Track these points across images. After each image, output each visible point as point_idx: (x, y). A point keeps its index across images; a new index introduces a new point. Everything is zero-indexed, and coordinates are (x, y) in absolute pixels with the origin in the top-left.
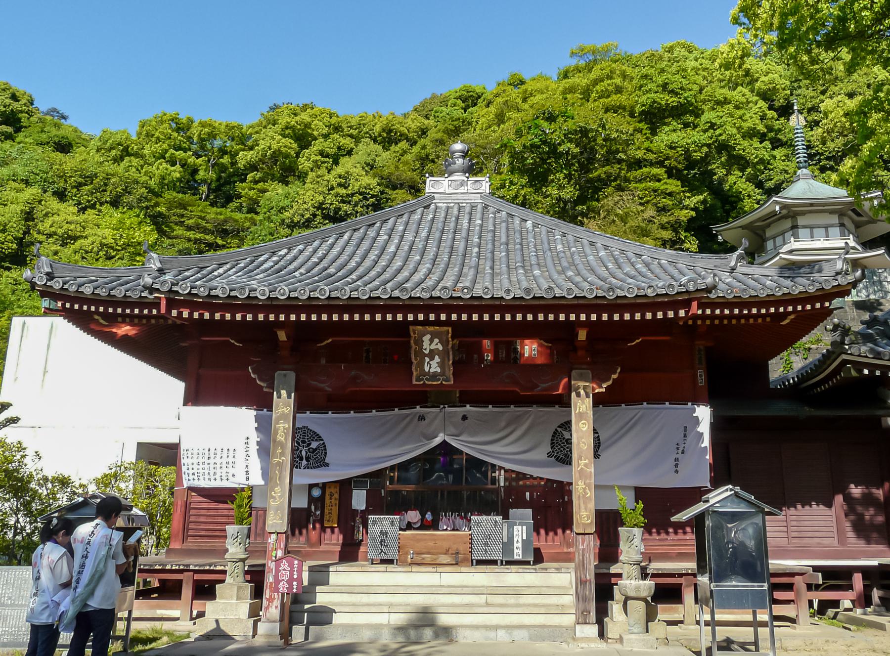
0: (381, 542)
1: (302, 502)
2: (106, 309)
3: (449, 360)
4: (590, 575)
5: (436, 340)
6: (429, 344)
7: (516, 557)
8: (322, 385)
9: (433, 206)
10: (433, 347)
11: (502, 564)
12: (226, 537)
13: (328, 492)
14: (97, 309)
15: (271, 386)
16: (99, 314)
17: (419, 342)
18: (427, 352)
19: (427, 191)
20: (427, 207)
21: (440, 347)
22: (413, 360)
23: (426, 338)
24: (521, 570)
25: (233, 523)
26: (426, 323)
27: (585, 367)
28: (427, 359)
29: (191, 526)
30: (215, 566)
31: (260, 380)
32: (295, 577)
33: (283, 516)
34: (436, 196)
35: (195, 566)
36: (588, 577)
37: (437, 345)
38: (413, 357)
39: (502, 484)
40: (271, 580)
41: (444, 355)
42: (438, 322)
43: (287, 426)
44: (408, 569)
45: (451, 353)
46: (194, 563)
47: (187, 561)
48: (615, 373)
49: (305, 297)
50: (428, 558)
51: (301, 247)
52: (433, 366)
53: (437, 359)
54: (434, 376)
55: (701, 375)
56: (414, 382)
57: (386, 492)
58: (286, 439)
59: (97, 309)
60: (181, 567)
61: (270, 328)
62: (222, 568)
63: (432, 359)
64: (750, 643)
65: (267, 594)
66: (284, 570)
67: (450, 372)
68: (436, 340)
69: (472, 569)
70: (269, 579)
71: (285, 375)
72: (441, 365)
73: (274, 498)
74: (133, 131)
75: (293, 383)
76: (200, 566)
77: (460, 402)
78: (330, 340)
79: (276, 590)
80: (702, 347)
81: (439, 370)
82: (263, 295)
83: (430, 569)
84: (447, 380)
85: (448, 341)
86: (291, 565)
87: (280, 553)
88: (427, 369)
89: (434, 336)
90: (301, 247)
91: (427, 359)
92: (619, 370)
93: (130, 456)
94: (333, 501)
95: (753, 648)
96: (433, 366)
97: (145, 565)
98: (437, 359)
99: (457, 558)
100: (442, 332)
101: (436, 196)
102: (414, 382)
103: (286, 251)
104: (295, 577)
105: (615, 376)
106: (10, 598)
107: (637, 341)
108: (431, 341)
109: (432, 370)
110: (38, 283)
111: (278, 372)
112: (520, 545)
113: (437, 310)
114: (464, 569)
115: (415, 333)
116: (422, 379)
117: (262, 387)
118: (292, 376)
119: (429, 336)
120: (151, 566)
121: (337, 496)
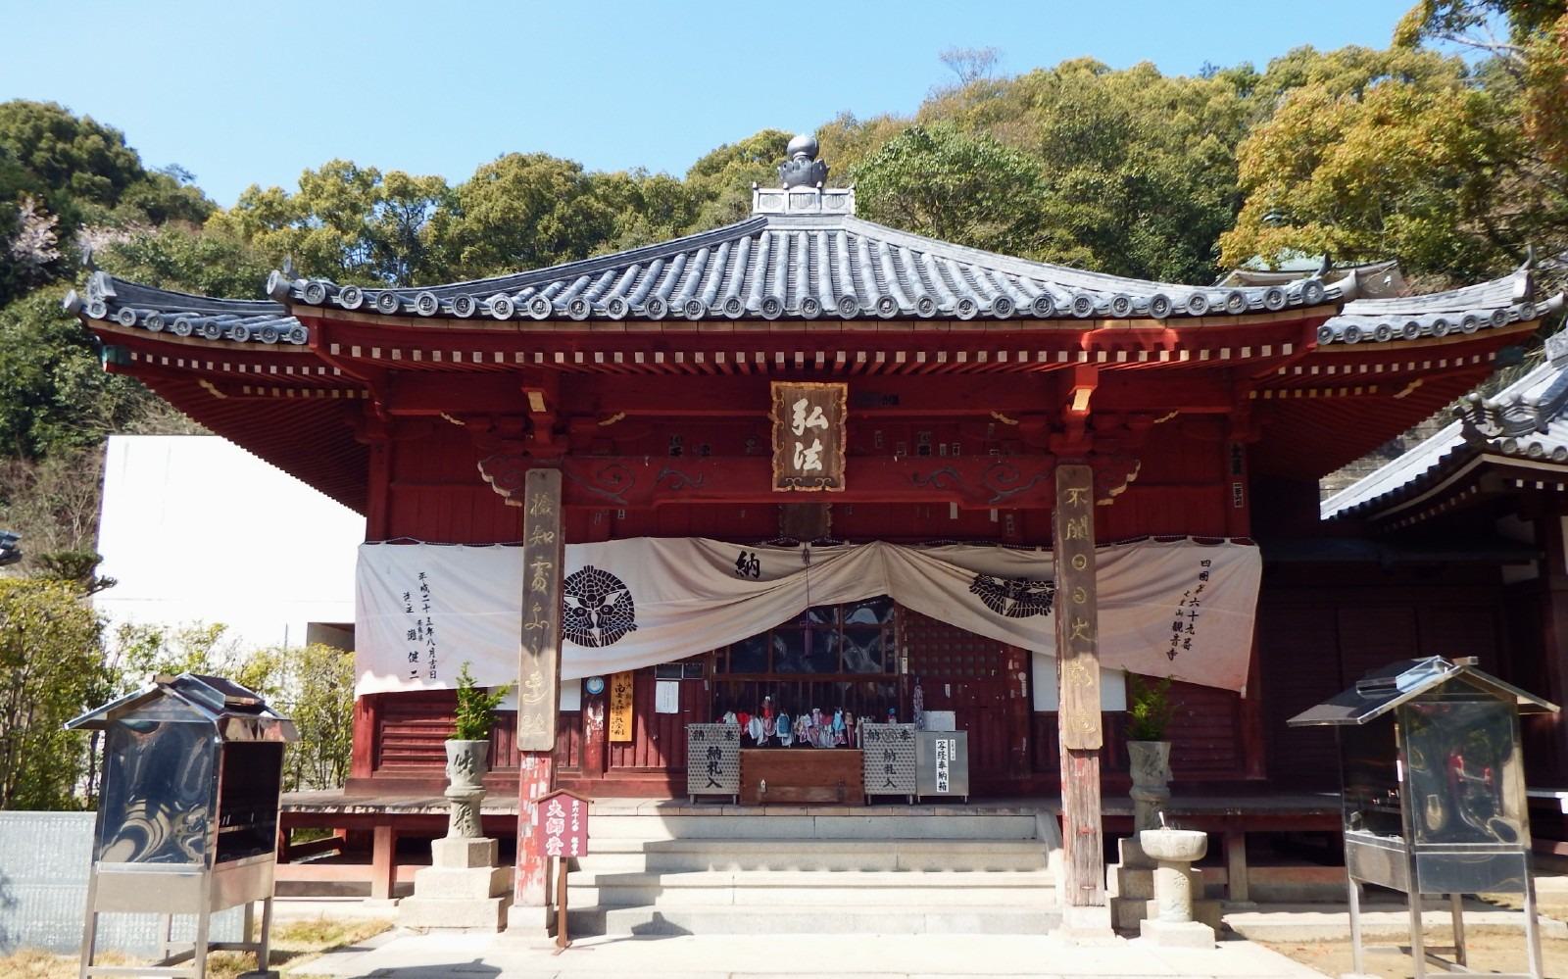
0: (710, 767)
1: (572, 703)
2: (218, 366)
3: (839, 448)
4: (1094, 822)
5: (818, 410)
6: (806, 416)
7: (939, 791)
8: (612, 495)
9: (765, 236)
10: (811, 423)
11: (915, 802)
12: (445, 760)
13: (614, 685)
14: (202, 365)
15: (519, 495)
16: (209, 377)
17: (786, 414)
18: (799, 432)
19: (755, 210)
20: (757, 236)
21: (824, 423)
22: (775, 448)
23: (800, 407)
24: (951, 812)
25: (455, 737)
26: (791, 373)
27: (1078, 460)
28: (799, 446)
29: (388, 742)
30: (429, 808)
31: (499, 485)
32: (575, 828)
33: (546, 723)
34: (769, 218)
35: (395, 808)
36: (1091, 825)
37: (819, 420)
38: (774, 441)
39: (905, 671)
40: (529, 833)
41: (829, 437)
42: (828, 373)
43: (550, 566)
44: (759, 811)
45: (844, 433)
46: (394, 803)
47: (380, 800)
48: (1132, 471)
49: (582, 317)
50: (791, 792)
51: (557, 285)
52: (809, 459)
53: (817, 446)
54: (811, 478)
55: (1238, 491)
56: (775, 489)
57: (712, 684)
58: (548, 588)
59: (202, 365)
60: (371, 810)
61: (517, 380)
62: (440, 811)
63: (808, 445)
64: (1447, 950)
65: (522, 856)
66: (555, 816)
67: (838, 472)
68: (818, 410)
69: (868, 811)
70: (525, 833)
71: (543, 476)
72: (825, 457)
73: (530, 691)
74: (294, 192)
75: (558, 490)
76: (403, 808)
77: (834, 535)
78: (622, 415)
79: (542, 850)
80: (1240, 445)
81: (819, 466)
82: (504, 311)
83: (796, 811)
84: (834, 485)
85: (841, 411)
86: (567, 809)
87: (544, 787)
88: (797, 464)
89: (814, 400)
90: (557, 285)
91: (799, 446)
92: (1138, 468)
93: (299, 639)
94: (623, 700)
95: (1452, 958)
96: (809, 459)
97: (308, 807)
98: (817, 446)
99: (840, 792)
100: (827, 395)
101: (769, 218)
102: (775, 489)
103: (530, 290)
104: (575, 828)
105: (1131, 477)
106: (54, 869)
107: (1172, 415)
108: (809, 411)
109: (806, 467)
110: (93, 315)
111: (532, 470)
112: (946, 770)
113: (831, 343)
114: (854, 811)
115: (779, 396)
116: (790, 483)
117: (502, 498)
118: (555, 477)
119: (803, 403)
120: (319, 808)
121: (630, 691)
